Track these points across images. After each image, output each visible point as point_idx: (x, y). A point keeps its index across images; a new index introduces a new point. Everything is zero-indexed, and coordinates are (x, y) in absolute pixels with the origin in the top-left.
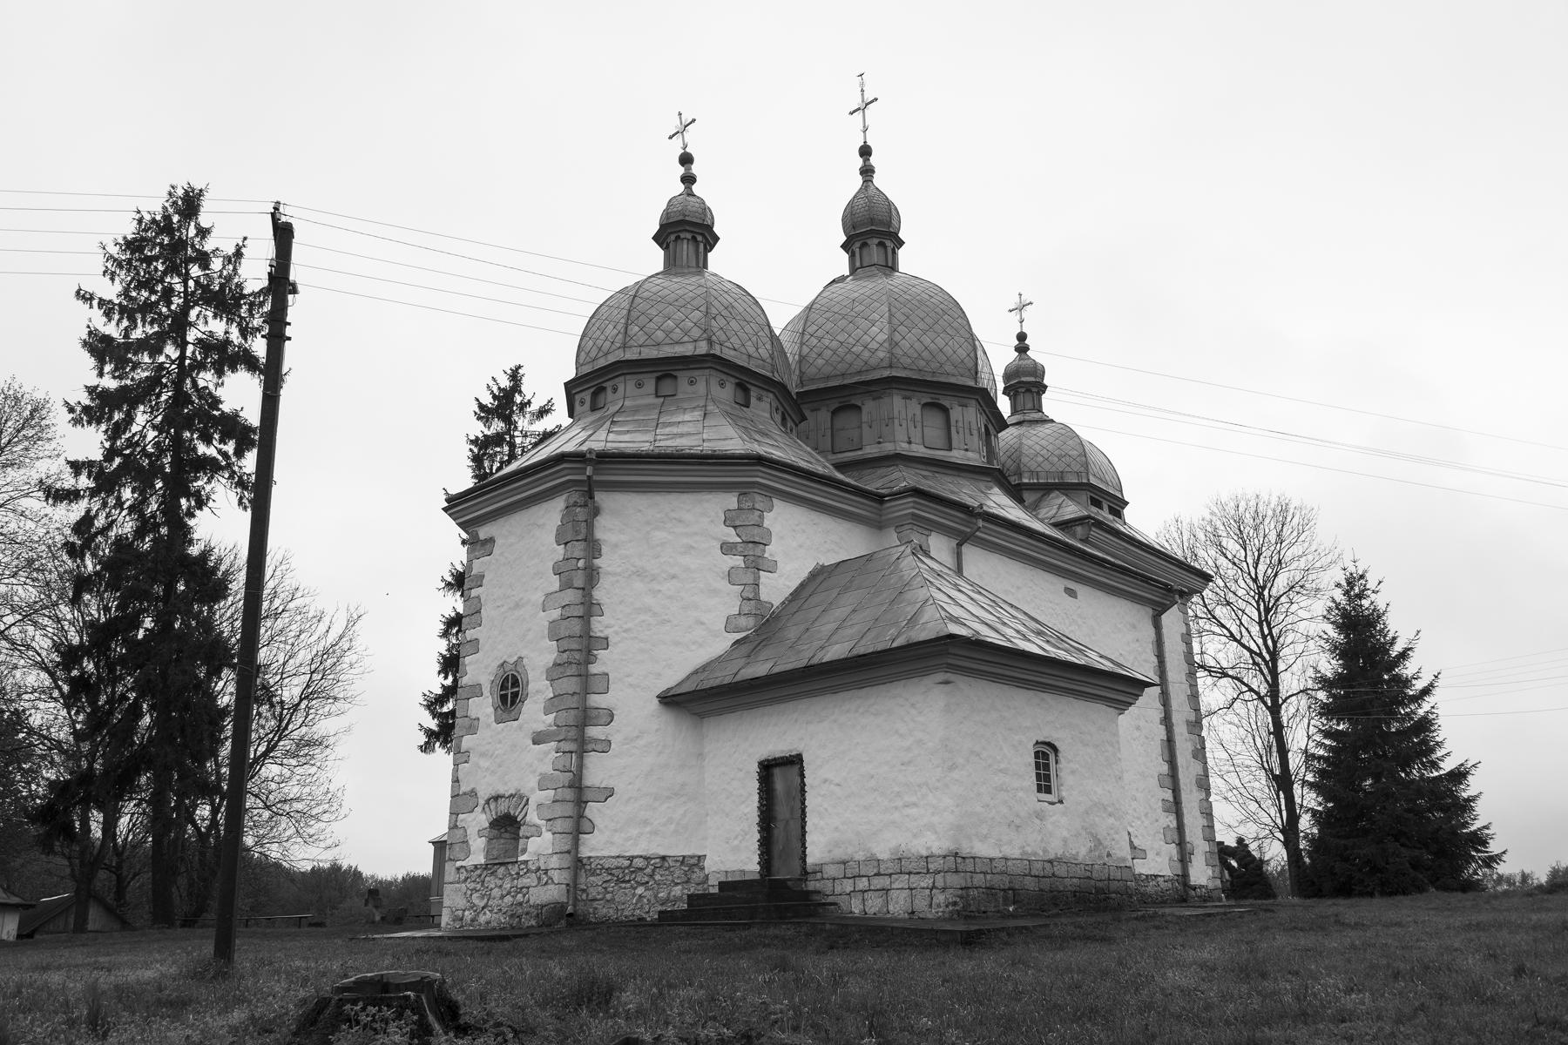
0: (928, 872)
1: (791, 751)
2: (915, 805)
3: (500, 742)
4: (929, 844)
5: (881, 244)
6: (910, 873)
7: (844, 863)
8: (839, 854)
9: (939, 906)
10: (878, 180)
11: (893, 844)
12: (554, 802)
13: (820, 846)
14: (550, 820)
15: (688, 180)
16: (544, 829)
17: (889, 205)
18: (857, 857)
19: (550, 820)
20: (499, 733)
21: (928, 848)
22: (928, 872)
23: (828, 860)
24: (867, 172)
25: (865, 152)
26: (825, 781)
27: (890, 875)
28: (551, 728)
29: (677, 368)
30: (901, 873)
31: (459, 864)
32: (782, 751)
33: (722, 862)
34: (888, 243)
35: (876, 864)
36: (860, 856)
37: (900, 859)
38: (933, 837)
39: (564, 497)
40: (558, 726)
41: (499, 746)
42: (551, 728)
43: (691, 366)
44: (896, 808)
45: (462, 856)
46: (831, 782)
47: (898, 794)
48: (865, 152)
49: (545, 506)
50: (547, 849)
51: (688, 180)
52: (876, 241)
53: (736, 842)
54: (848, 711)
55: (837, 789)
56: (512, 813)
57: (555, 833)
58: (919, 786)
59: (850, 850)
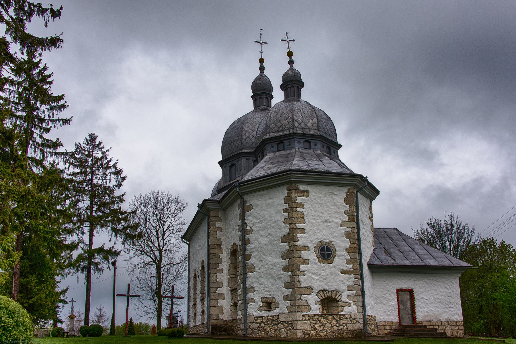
0: (457, 325)
1: (409, 288)
2: (452, 308)
3: (324, 270)
4: (457, 318)
5: (267, 98)
6: (451, 325)
7: (430, 321)
8: (427, 319)
9: (460, 334)
10: (266, 72)
11: (446, 317)
12: (355, 295)
13: (420, 316)
14: (355, 301)
15: (291, 63)
16: (352, 304)
17: (271, 86)
18: (434, 320)
19: (355, 301)
20: (323, 267)
21: (457, 319)
22: (457, 325)
23: (424, 320)
24: (262, 69)
25: (262, 61)
26: (422, 298)
27: (445, 325)
28: (351, 270)
29: (332, 145)
30: (449, 325)
31: (304, 313)
32: (406, 288)
33: (383, 319)
34: (269, 98)
35: (441, 322)
36: (435, 320)
37: (448, 321)
38: (458, 316)
39: (348, 188)
40: (354, 269)
41: (323, 272)
42: (351, 270)
43: (335, 147)
44: (446, 308)
45: (306, 310)
46: (424, 299)
47: (447, 304)
48: (262, 61)
49: (341, 188)
50: (355, 311)
51: (291, 63)
52: (265, 97)
53: (389, 313)
54: (429, 279)
55: (426, 301)
56: (334, 297)
57: (358, 306)
58: (454, 303)
59: (432, 318)
